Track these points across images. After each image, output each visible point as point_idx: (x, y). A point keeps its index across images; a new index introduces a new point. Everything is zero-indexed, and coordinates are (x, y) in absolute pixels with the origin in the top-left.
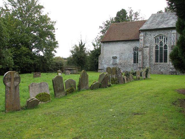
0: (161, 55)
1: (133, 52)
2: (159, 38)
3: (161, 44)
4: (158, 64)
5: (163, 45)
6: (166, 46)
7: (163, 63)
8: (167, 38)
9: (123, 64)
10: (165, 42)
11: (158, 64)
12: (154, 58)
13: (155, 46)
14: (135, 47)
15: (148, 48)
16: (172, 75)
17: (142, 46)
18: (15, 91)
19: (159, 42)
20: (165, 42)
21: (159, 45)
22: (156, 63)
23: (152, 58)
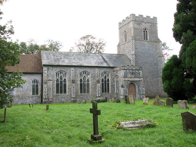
0: (61, 87)
1: (32, 84)
2: (83, 73)
3: (105, 79)
4: (59, 95)
5: (63, 79)
6: (65, 80)
7: (63, 94)
8: (66, 74)
9: (21, 96)
10: (64, 76)
11: (59, 95)
12: (55, 90)
13: (80, 80)
14: (35, 80)
15: (52, 81)
16: (74, 103)
17: (46, 79)
18: (139, 107)
19: (59, 76)
20: (64, 76)
21: (59, 79)
22: (57, 94)
23: (54, 90)
